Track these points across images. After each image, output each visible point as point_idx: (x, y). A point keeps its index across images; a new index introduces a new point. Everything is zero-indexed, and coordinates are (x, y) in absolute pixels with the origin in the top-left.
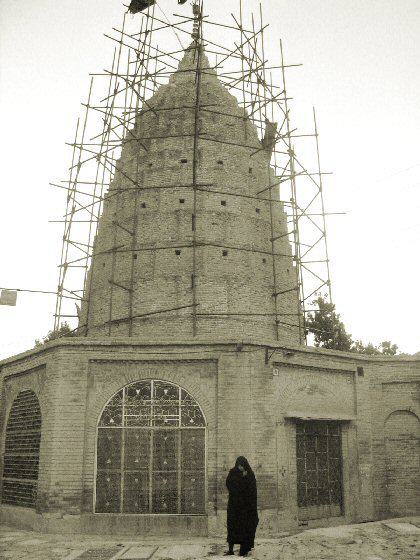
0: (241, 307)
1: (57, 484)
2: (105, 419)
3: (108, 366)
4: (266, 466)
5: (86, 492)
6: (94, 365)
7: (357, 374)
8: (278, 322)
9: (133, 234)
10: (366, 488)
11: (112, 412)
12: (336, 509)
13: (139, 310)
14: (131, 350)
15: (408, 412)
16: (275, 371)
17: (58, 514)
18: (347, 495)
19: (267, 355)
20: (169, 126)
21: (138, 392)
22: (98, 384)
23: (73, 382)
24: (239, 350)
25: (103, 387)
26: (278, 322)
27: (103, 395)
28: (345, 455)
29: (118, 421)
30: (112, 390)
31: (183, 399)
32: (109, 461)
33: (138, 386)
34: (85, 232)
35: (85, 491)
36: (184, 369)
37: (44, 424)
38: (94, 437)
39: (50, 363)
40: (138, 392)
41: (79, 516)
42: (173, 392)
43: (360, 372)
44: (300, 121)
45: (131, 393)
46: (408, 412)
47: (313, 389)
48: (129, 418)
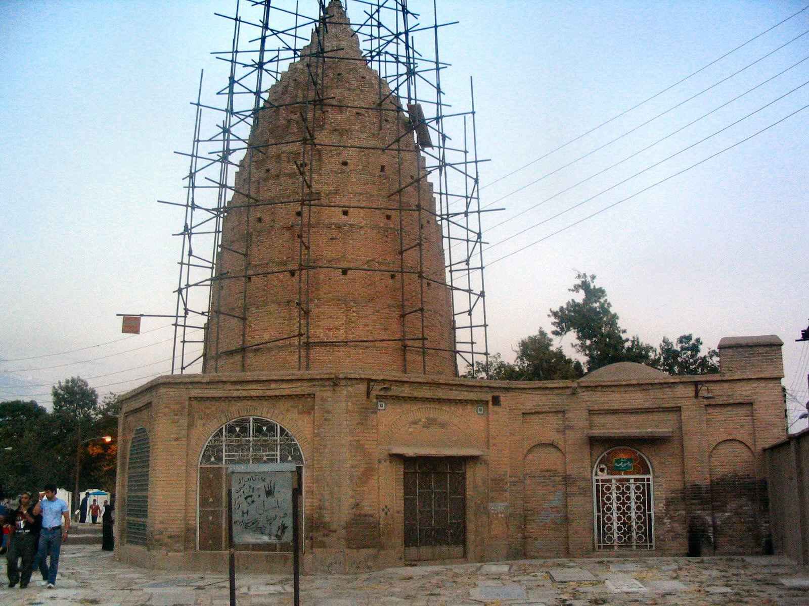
0: (360, 333)
1: (162, 522)
2: (206, 458)
3: (208, 404)
4: (365, 503)
5: (189, 530)
6: (195, 403)
7: (490, 403)
8: (405, 347)
9: (246, 255)
10: (498, 529)
11: (213, 451)
12: (459, 550)
13: (252, 340)
14: (229, 387)
15: (552, 445)
16: (382, 406)
17: (163, 551)
18: (471, 537)
19: (368, 388)
20: (289, 121)
21: (238, 429)
22: (199, 423)
23: (174, 422)
24: (335, 385)
25: (204, 425)
26: (405, 347)
27: (204, 432)
28: (469, 493)
29: (219, 459)
30: (213, 427)
31: (281, 435)
32: (211, 500)
33: (238, 423)
34: (206, 246)
35: (188, 530)
36: (282, 405)
37: (151, 464)
38: (196, 477)
39: (155, 401)
40: (238, 429)
41: (182, 554)
42: (271, 428)
43: (496, 401)
44: (456, 98)
45: (231, 430)
46: (552, 445)
47: (431, 422)
48: (229, 456)
